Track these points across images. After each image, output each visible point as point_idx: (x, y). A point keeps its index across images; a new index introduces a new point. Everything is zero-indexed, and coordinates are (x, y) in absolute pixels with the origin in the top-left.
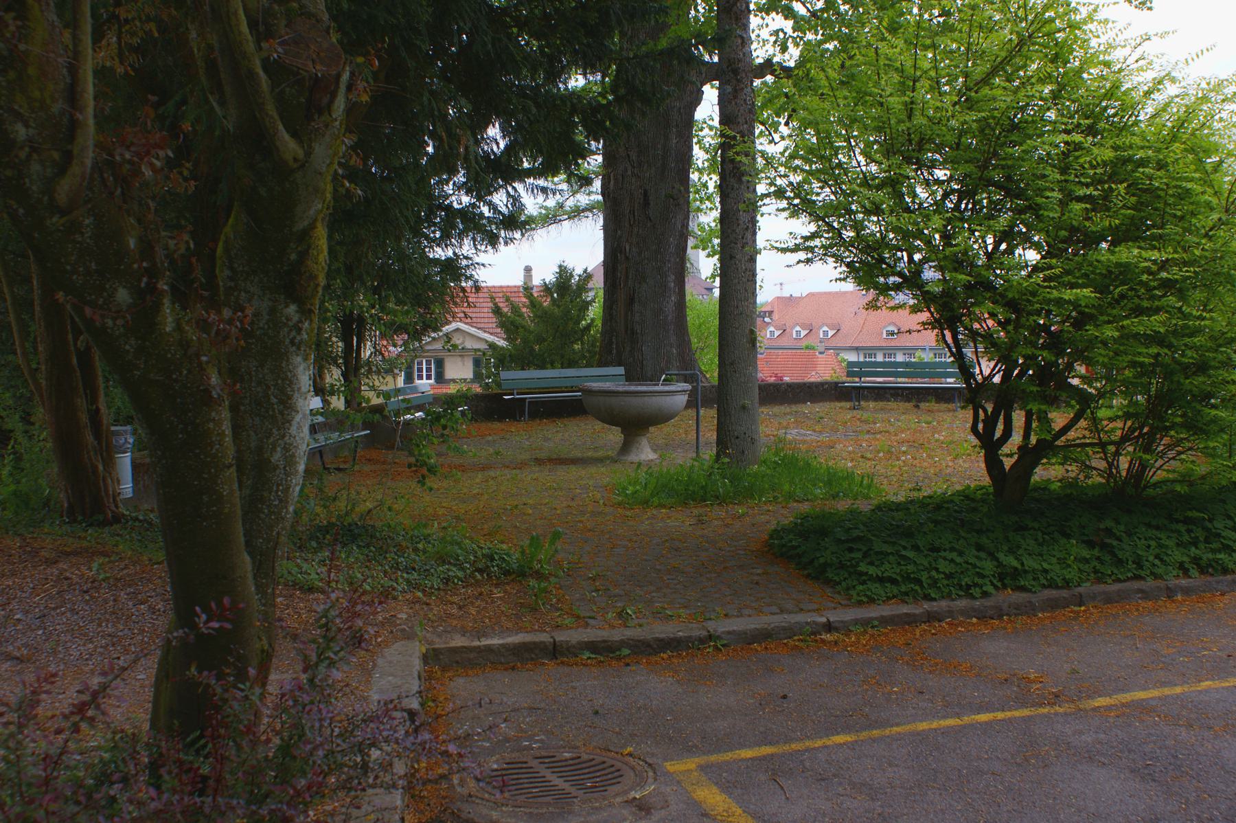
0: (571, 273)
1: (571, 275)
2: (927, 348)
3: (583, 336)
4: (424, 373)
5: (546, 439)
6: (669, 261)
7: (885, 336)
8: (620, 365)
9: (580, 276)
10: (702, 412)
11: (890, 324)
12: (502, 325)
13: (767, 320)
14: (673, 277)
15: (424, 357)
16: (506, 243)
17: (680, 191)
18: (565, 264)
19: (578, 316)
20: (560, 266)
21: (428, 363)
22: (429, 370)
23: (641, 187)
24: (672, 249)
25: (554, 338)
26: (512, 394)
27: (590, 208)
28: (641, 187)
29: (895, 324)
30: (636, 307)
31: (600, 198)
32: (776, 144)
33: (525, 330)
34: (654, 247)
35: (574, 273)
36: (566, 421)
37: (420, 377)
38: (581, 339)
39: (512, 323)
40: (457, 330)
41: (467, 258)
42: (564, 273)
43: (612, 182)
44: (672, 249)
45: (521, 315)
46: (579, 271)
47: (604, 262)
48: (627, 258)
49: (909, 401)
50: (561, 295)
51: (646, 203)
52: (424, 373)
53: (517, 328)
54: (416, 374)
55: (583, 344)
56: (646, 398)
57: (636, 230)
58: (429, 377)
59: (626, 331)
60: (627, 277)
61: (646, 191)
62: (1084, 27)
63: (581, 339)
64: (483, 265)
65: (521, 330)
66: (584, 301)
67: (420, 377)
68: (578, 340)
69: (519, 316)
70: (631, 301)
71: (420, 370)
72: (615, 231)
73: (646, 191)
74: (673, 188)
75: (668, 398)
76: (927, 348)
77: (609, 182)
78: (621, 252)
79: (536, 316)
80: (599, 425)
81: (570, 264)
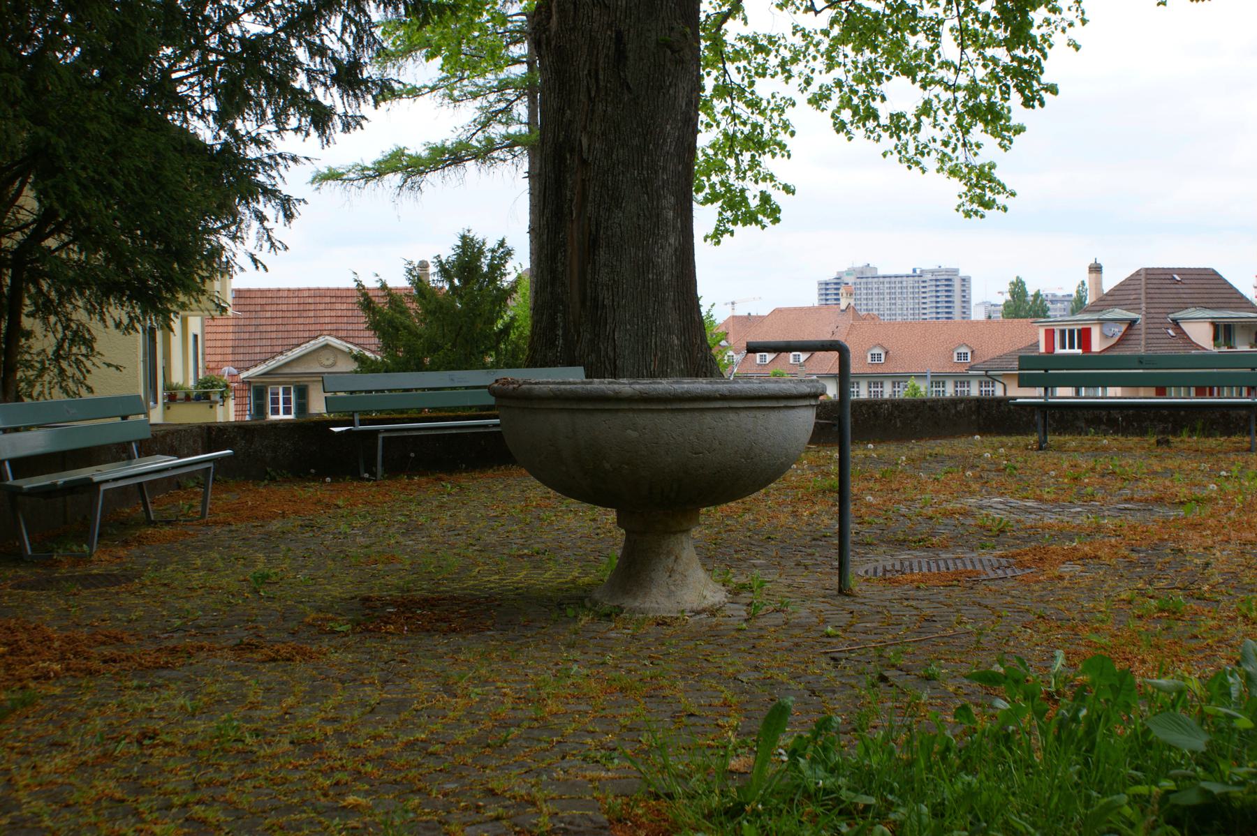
0: (480, 249)
1: (481, 252)
2: (929, 375)
3: (498, 343)
4: (281, 406)
5: (411, 529)
6: (664, 169)
7: (869, 360)
8: (571, 363)
9: (493, 251)
10: (857, 453)
11: (875, 346)
12: (374, 326)
13: (723, 343)
14: (672, 200)
15: (279, 383)
16: (347, 127)
17: (685, 35)
18: (471, 235)
19: (491, 312)
20: (463, 237)
21: (286, 391)
22: (287, 401)
23: (610, 26)
24: (670, 147)
25: (454, 345)
26: (351, 423)
27: (512, 143)
28: (610, 26)
29: (882, 346)
30: (603, 255)
31: (525, 129)
32: (817, 13)
33: (410, 332)
34: (636, 142)
35: (485, 249)
36: (464, 479)
37: (276, 411)
38: (496, 348)
39: (391, 323)
40: (327, 346)
41: (257, 141)
42: (469, 249)
43: (554, 18)
44: (670, 147)
45: (404, 312)
46: (491, 243)
47: (531, 269)
48: (584, 162)
49: (1142, 432)
50: (466, 281)
51: (620, 55)
52: (281, 406)
53: (398, 330)
54: (269, 406)
55: (498, 354)
56: (708, 418)
57: (600, 107)
58: (287, 411)
59: (583, 303)
60: (584, 197)
61: (619, 35)
62: (190, 709)
63: (496, 348)
64: (294, 159)
65: (403, 332)
66: (499, 289)
67: (276, 411)
68: (489, 349)
69: (401, 313)
70: (592, 244)
71: (275, 401)
72: (561, 111)
73: (619, 35)
74: (672, 29)
75: (774, 416)
76: (929, 375)
77: (549, 18)
78: (572, 151)
79: (428, 312)
80: (536, 490)
81: (478, 234)
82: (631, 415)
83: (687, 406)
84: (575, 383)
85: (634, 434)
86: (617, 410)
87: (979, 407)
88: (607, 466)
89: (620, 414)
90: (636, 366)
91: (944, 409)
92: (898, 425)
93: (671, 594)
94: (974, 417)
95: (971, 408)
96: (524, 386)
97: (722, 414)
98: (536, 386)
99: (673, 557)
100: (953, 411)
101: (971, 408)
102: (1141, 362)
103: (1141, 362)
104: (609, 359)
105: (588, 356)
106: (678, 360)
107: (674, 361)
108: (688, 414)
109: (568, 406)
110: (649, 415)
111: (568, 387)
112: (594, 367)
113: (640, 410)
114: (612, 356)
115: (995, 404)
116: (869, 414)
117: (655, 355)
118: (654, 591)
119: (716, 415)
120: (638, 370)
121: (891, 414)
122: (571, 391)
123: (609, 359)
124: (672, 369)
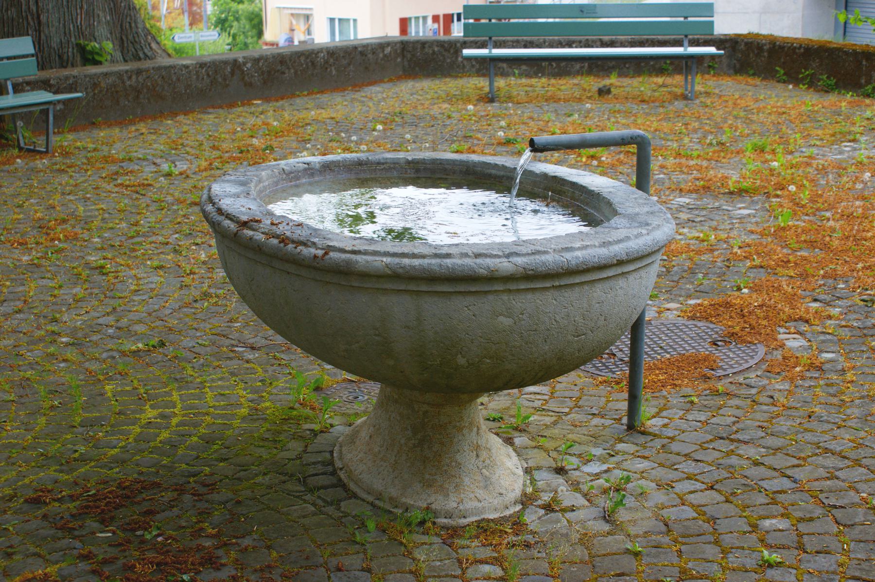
82: (505, 297)
83: (578, 280)
84: (423, 257)
85: (505, 321)
86: (486, 293)
87: (403, 49)
88: (461, 361)
89: (491, 297)
90: (62, 22)
91: (374, 53)
92: (334, 72)
93: (487, 482)
94: (399, 60)
95: (396, 50)
96: (332, 254)
97: (612, 283)
98: (359, 258)
99: (475, 429)
100: (381, 55)
101: (396, 50)
102: (582, 11)
103: (582, 11)
104: (32, 15)
105: (7, 10)
106: (104, 11)
107: (101, 14)
108: (577, 289)
109: (412, 287)
110: (529, 296)
111: (416, 262)
112: (15, 23)
113: (518, 291)
114: (35, 10)
115: (419, 46)
116: (307, 64)
117: (81, 8)
118: (467, 480)
119: (607, 285)
120: (64, 25)
121: (326, 62)
122: (423, 269)
123: (32, 15)
124: (99, 22)
